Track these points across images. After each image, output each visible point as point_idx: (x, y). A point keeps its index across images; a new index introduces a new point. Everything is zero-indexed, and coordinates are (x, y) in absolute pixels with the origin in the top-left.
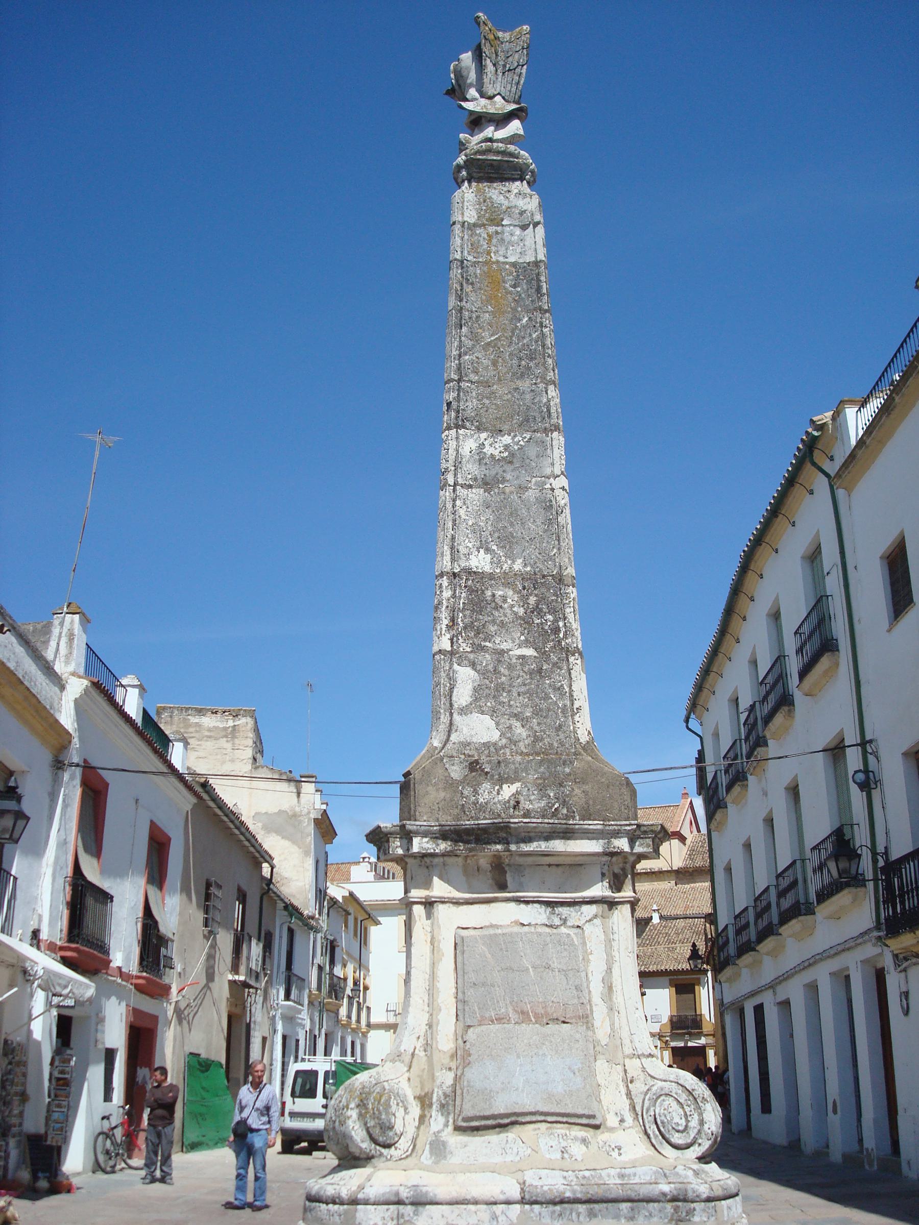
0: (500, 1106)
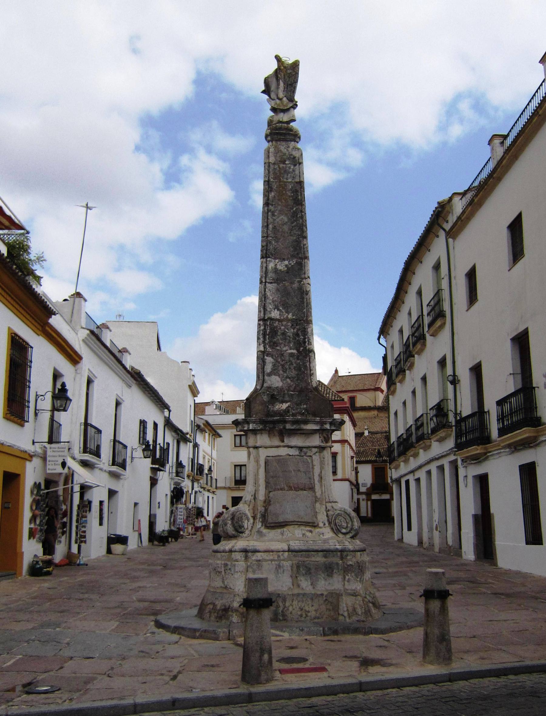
0: (281, 519)
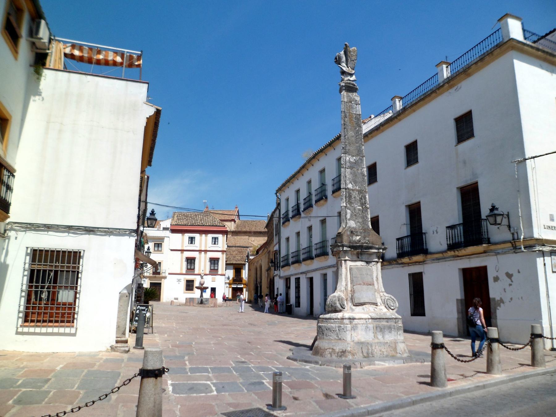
0: (362, 301)
